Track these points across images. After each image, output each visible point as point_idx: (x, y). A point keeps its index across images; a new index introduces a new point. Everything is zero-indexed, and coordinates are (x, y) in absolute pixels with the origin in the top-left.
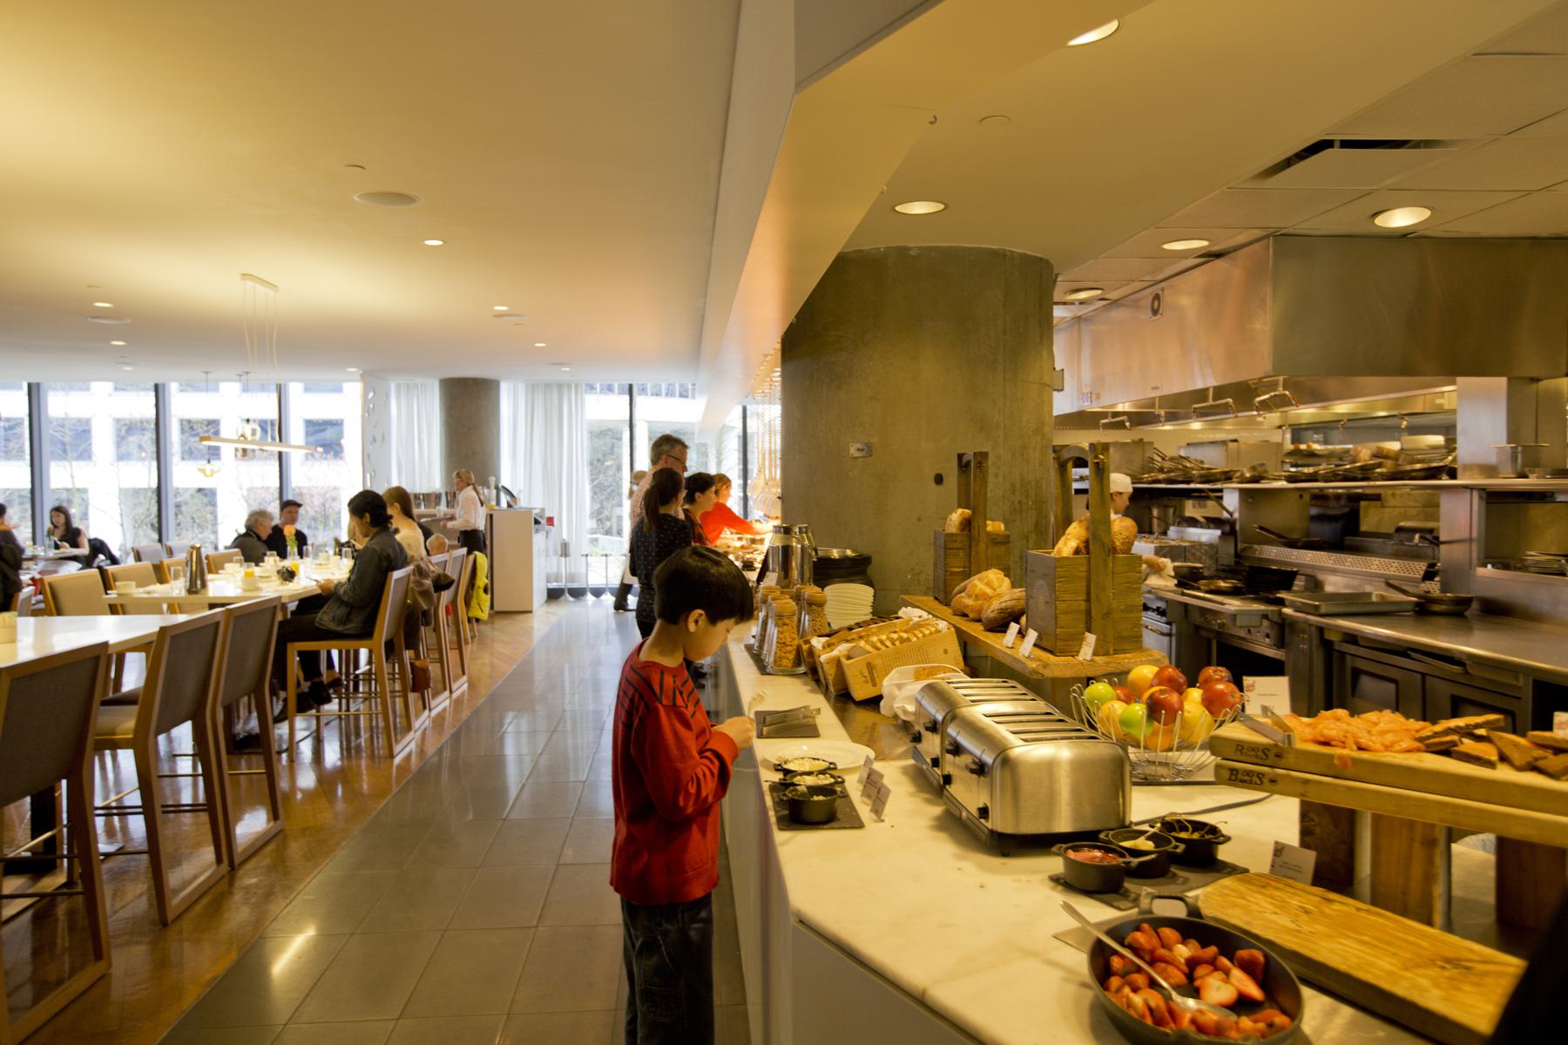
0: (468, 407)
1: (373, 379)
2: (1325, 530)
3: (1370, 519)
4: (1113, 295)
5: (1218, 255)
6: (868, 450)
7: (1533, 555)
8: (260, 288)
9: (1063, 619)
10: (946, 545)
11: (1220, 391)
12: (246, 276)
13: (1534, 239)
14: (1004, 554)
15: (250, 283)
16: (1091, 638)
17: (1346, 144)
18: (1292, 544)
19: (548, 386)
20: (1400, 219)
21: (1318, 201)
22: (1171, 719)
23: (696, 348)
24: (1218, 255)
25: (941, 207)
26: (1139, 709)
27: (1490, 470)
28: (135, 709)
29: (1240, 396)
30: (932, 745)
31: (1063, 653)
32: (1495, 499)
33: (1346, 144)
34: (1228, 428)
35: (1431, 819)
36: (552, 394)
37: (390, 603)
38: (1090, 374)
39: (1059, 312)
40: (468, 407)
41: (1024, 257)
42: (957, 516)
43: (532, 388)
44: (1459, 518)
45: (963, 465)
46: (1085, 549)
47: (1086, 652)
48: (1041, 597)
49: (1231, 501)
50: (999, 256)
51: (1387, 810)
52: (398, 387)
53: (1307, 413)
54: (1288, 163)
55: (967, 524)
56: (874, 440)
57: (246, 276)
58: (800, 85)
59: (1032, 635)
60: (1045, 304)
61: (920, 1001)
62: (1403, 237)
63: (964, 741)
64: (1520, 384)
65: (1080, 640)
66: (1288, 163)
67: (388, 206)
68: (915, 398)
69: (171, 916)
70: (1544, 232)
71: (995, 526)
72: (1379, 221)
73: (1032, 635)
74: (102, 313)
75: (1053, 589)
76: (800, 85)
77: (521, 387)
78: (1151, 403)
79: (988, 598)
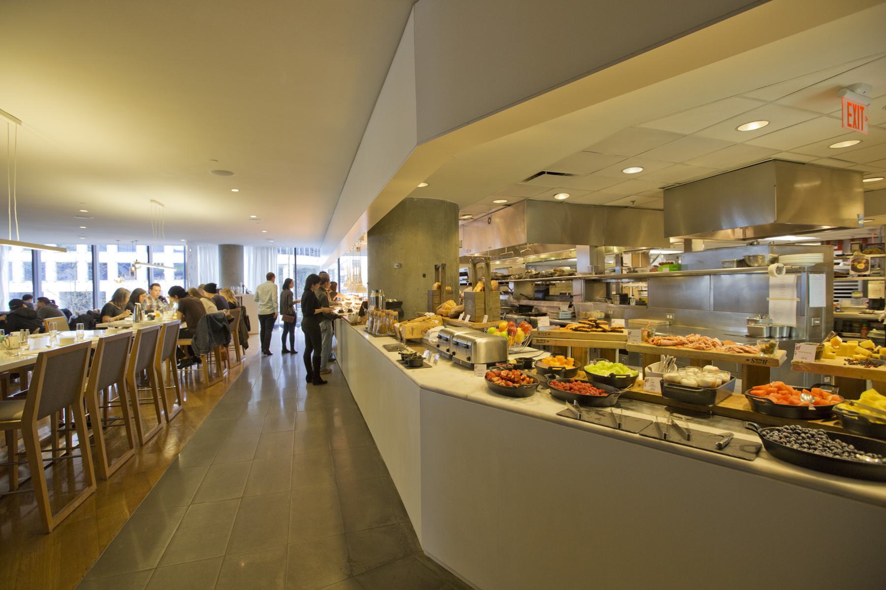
0: (230, 256)
1: (191, 243)
2: (540, 295)
3: (553, 291)
4: (475, 218)
5: (509, 205)
6: (400, 266)
7: (598, 298)
8: (158, 206)
9: (478, 311)
10: (432, 294)
11: (502, 250)
12: (152, 201)
13: (595, 206)
14: (454, 295)
15: (154, 204)
16: (486, 317)
17: (549, 173)
18: (530, 299)
19: (262, 248)
20: (562, 197)
21: (539, 191)
22: (514, 335)
23: (326, 234)
24: (509, 205)
25: (625, 171)
26: (505, 333)
27: (585, 274)
28: (23, 403)
29: (515, 251)
30: (443, 349)
31: (478, 321)
32: (589, 282)
33: (549, 173)
34: (508, 262)
35: (586, 346)
36: (264, 250)
37: (210, 326)
38: (474, 242)
39: (460, 223)
40: (230, 256)
41: (451, 203)
42: (436, 285)
43: (256, 248)
44: (578, 288)
45: (437, 269)
46: (484, 289)
47: (485, 320)
48: (470, 307)
49: (511, 286)
50: (443, 202)
51: (576, 345)
52: (200, 248)
53: (532, 258)
54: (532, 178)
55: (439, 287)
56: (402, 263)
57: (152, 201)
58: (418, 144)
59: (468, 317)
60: (457, 220)
61: (466, 399)
62: (561, 203)
63: (459, 341)
64: (593, 247)
65: (482, 317)
66: (532, 178)
67: (221, 175)
68: (414, 247)
69: (144, 442)
70: (597, 203)
71: (448, 288)
72: (556, 197)
73: (468, 317)
74: (83, 215)
75: (474, 302)
76: (418, 144)
77: (252, 248)
78: (486, 253)
79: (449, 309)
